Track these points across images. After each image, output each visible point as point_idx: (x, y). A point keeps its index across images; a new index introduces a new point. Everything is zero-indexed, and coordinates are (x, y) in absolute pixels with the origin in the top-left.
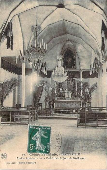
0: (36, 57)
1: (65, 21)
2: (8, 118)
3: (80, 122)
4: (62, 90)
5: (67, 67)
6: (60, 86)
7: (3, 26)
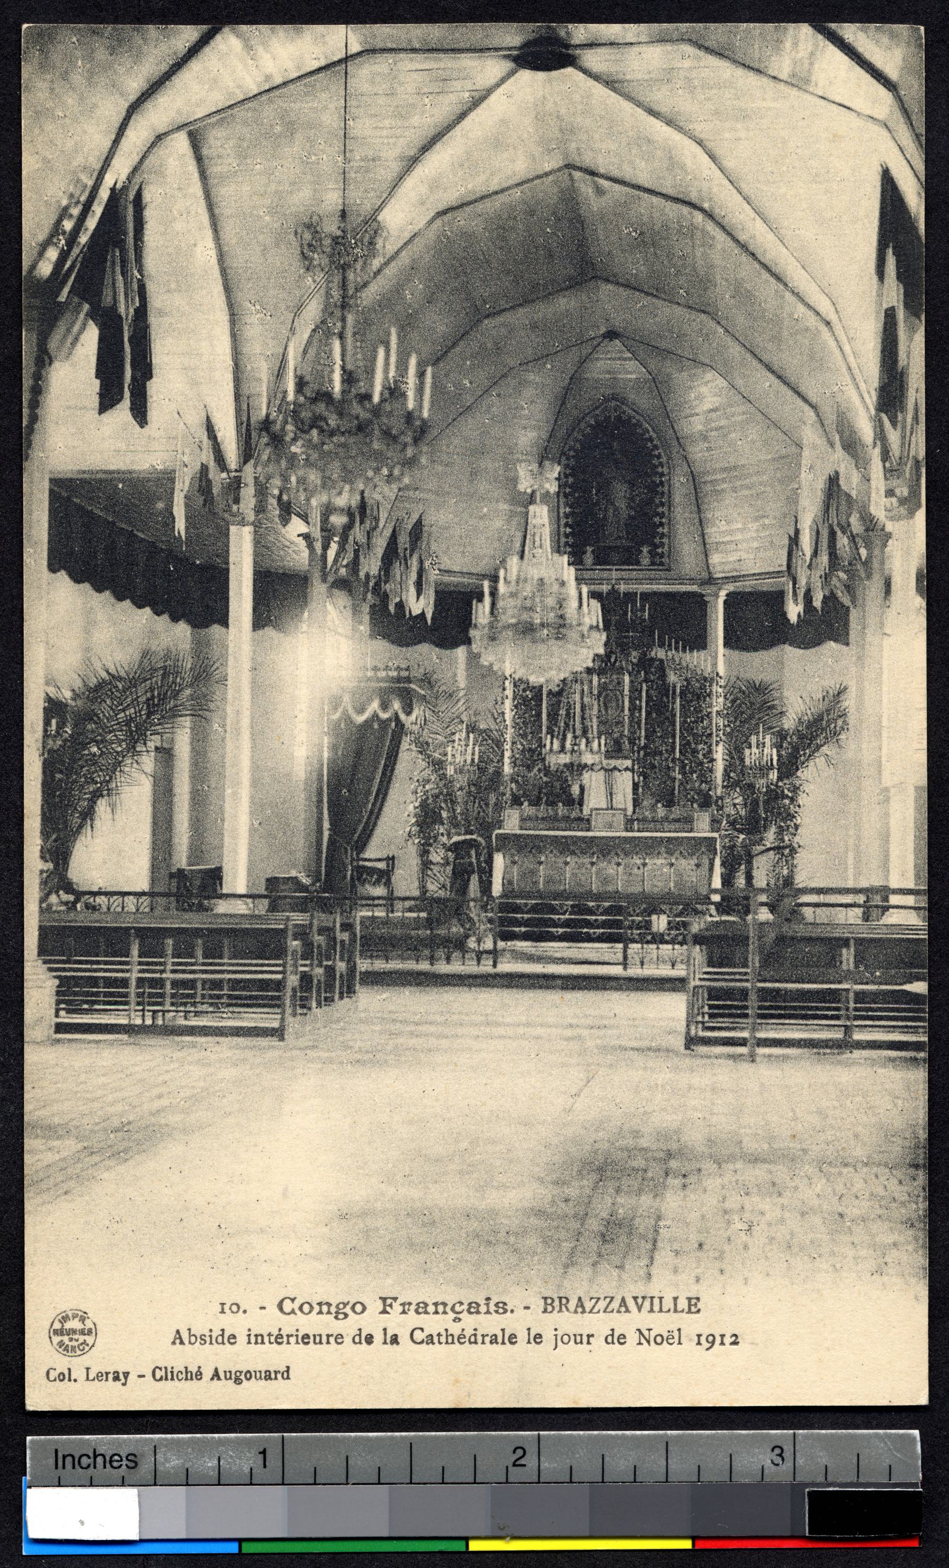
0: (335, 468)
1: (577, 175)
2: (109, 982)
3: (711, 1007)
4: (556, 745)
5: (602, 559)
6: (544, 716)
7: (68, 225)
